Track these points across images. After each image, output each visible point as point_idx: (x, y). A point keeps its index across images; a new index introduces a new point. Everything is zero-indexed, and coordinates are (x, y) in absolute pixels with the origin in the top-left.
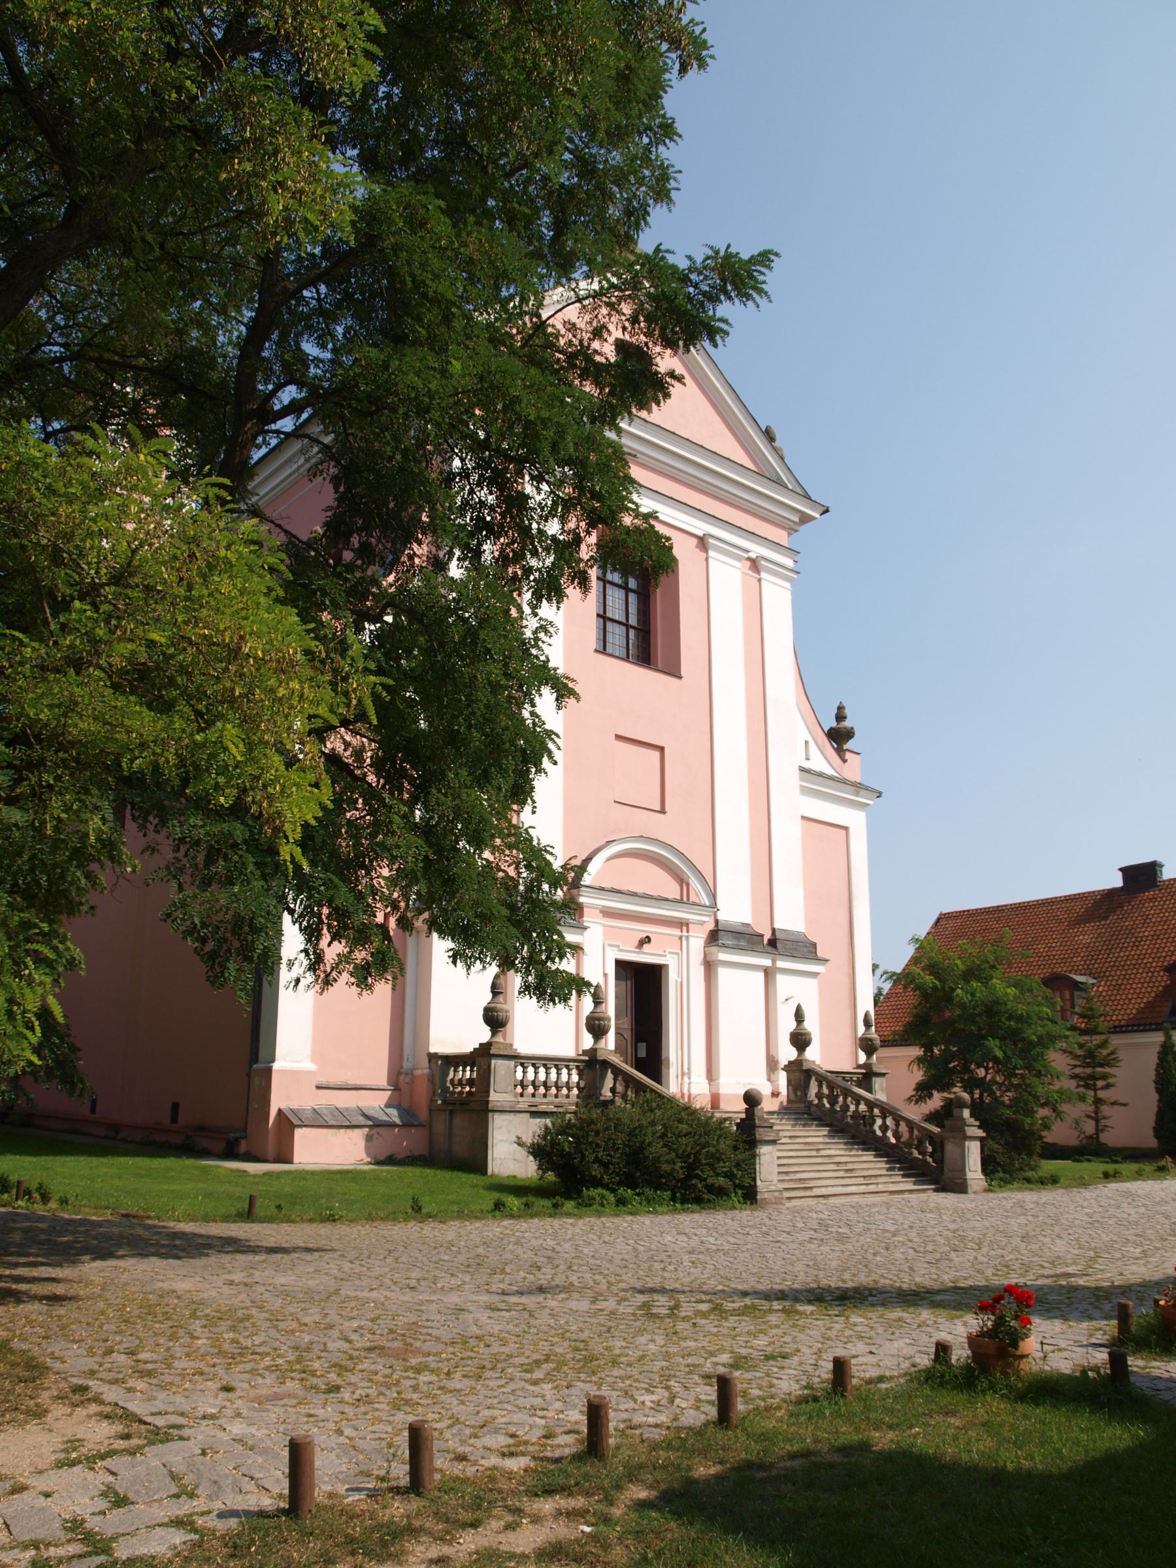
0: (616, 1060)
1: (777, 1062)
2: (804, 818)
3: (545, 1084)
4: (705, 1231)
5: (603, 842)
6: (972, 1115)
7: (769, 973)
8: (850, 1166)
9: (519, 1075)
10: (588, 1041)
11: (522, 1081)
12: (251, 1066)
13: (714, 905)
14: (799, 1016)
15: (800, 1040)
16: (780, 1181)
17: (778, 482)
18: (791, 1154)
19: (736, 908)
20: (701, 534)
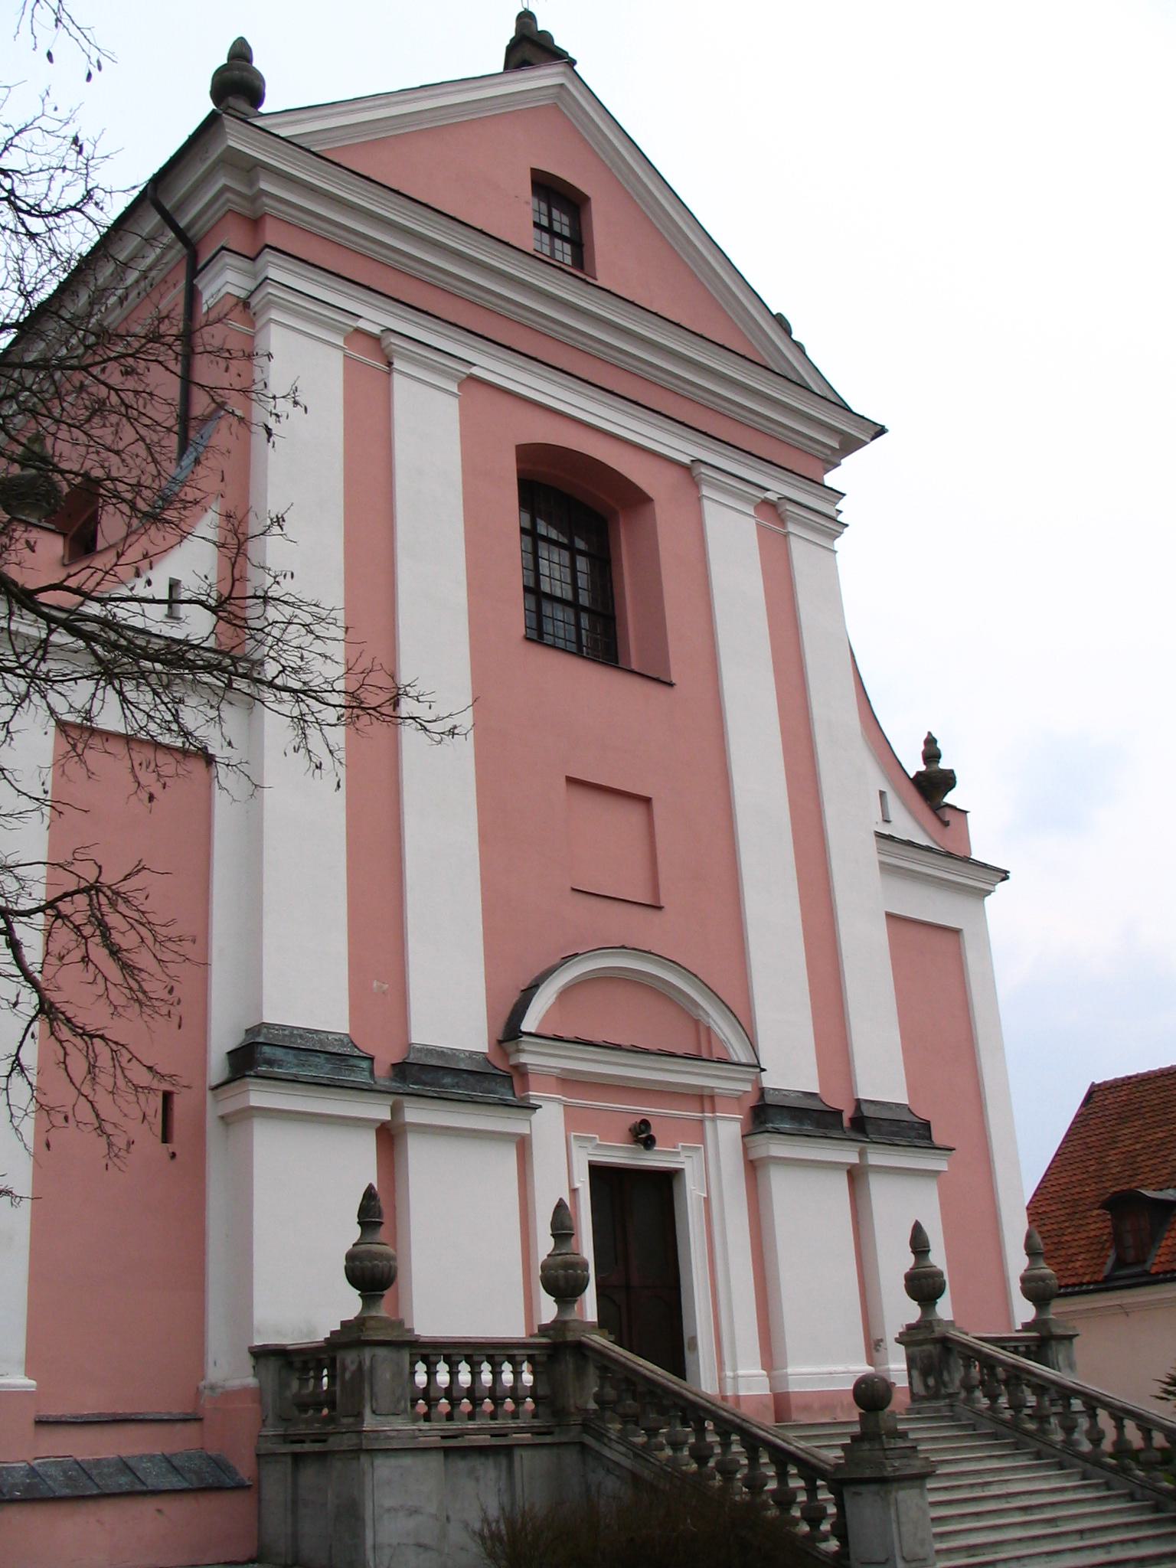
0: (599, 1340)
2: (570, 780)
3: (448, 1392)
5: (557, 960)
7: (856, 1176)
9: (421, 1379)
10: (548, 1309)
11: (426, 1390)
19: (792, 1068)
20: (686, 460)
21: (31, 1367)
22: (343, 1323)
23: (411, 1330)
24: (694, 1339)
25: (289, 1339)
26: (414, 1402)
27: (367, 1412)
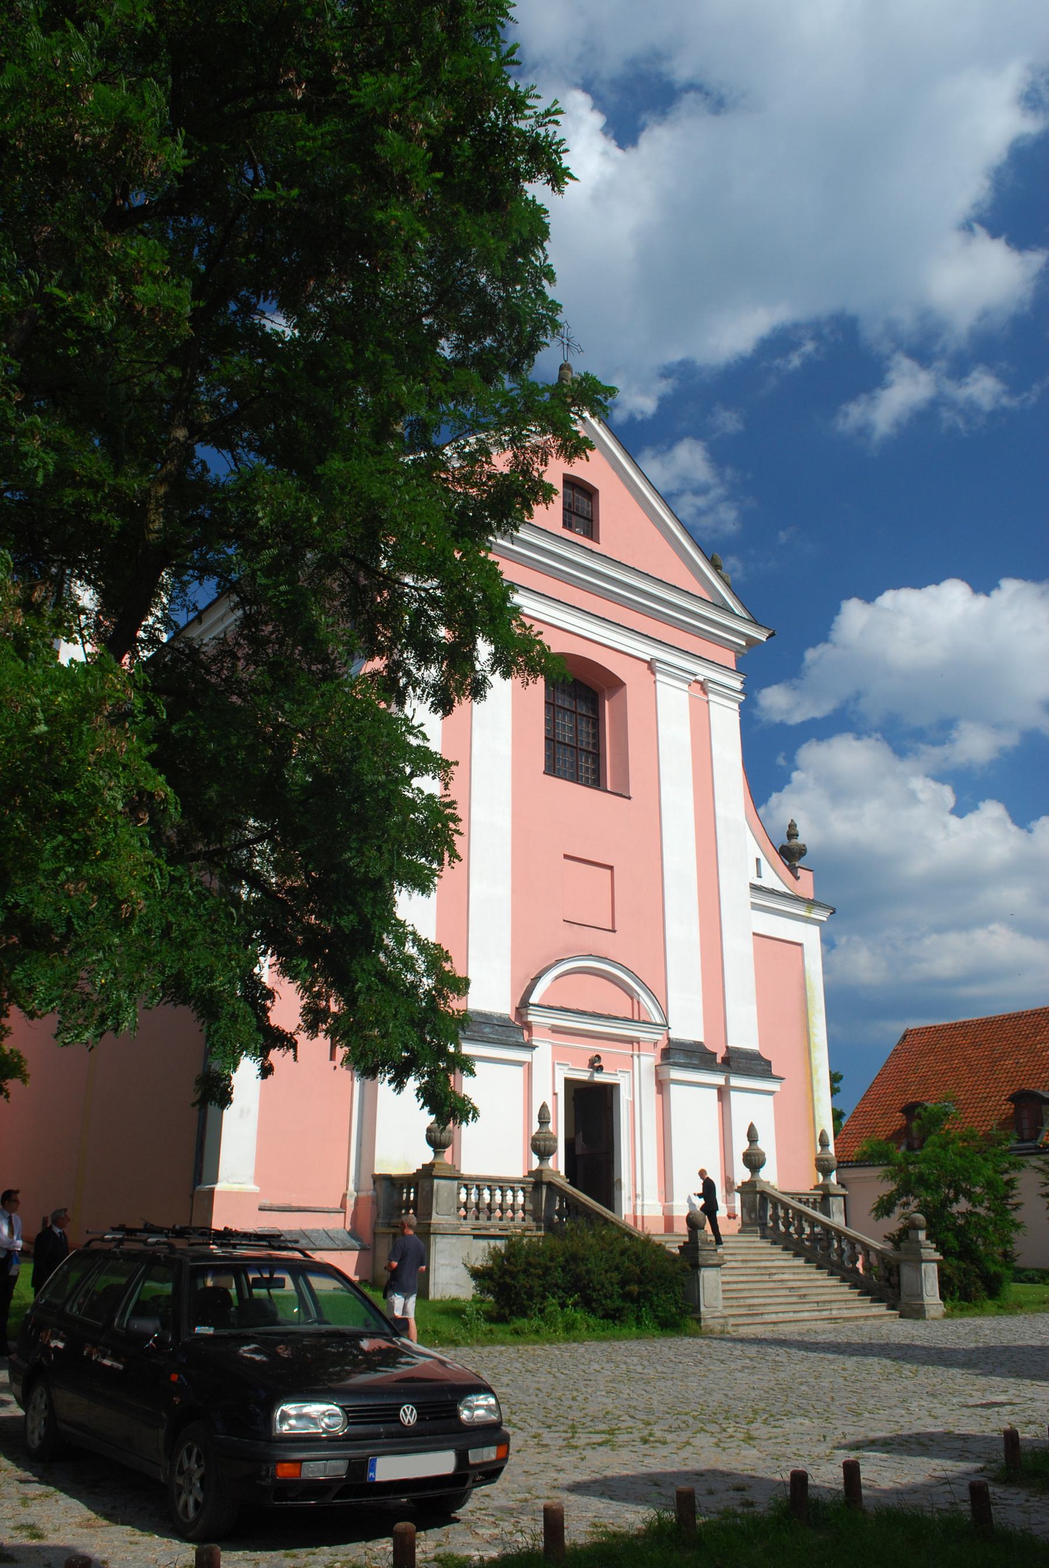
1: (733, 1183)
2: (754, 934)
4: (636, 1360)
6: (928, 1238)
7: (723, 1093)
8: (803, 1292)
9: (463, 1197)
11: (465, 1204)
12: (194, 1188)
13: (666, 1025)
14: (752, 1135)
15: (754, 1161)
16: (725, 1307)
17: (730, 611)
18: (742, 1278)
19: (688, 1026)
20: (648, 658)
21: (258, 1179)
22: (423, 1165)
23: (459, 1171)
24: (620, 1180)
25: (395, 1171)
26: (459, 1209)
27: (434, 1213)
